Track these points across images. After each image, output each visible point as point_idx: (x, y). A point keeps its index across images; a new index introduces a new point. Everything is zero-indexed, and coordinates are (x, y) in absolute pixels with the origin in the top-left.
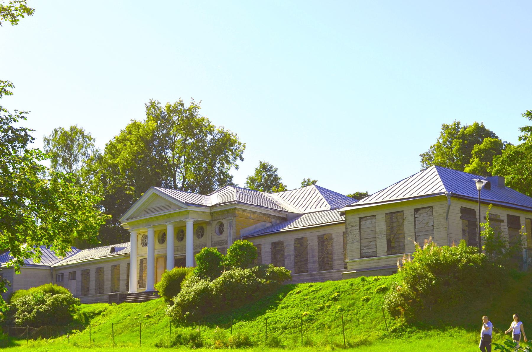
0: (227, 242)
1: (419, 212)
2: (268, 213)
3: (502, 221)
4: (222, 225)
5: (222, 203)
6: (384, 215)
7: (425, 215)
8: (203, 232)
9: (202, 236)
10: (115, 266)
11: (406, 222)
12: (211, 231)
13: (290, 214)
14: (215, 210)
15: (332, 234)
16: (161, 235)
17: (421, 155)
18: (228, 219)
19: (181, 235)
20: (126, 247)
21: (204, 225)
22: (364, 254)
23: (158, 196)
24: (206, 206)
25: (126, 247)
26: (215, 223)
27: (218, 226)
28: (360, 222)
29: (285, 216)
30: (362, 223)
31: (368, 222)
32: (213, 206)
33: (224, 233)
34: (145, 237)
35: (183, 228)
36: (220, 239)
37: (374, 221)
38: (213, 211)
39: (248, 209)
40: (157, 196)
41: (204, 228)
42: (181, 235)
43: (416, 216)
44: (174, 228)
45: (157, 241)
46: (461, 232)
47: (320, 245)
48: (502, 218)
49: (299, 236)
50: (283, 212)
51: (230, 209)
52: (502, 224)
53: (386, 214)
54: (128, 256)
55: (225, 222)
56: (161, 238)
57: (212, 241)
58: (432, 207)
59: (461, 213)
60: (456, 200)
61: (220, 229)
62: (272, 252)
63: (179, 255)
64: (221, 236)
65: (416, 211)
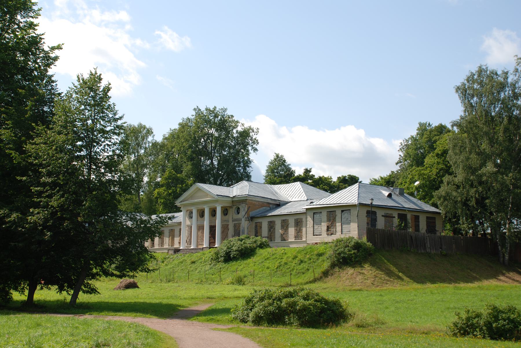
0: (241, 219)
1: (344, 212)
2: (267, 201)
3: (394, 217)
4: (239, 208)
5: (239, 196)
6: (326, 212)
7: (346, 214)
8: (227, 212)
9: (227, 214)
10: (172, 230)
11: (337, 218)
12: (232, 213)
13: (282, 202)
14: (235, 199)
15: (302, 219)
16: (201, 212)
17: (411, 135)
18: (242, 205)
19: (213, 213)
20: (178, 217)
21: (228, 208)
22: (315, 234)
23: (200, 189)
24: (229, 197)
25: (178, 217)
26: (235, 207)
27: (237, 209)
28: (314, 215)
29: (278, 203)
30: (314, 216)
31: (318, 215)
32: (234, 197)
33: (240, 213)
34: (191, 213)
35: (215, 209)
36: (237, 217)
37: (321, 215)
38: (233, 200)
39: (255, 199)
40: (199, 190)
41: (228, 209)
42: (213, 213)
43: (342, 214)
44: (197, 211)
45: (199, 216)
46: (366, 224)
47: (296, 225)
48: (394, 216)
49: (284, 218)
50: (277, 201)
51: (244, 200)
52: (394, 219)
53: (327, 212)
54: (180, 224)
55: (240, 207)
56: (201, 214)
57: (232, 218)
58: (350, 210)
59: (367, 213)
60: (129, 315)
61: (237, 211)
62: (268, 227)
63: (213, 224)
64: (238, 215)
65: (342, 211)
